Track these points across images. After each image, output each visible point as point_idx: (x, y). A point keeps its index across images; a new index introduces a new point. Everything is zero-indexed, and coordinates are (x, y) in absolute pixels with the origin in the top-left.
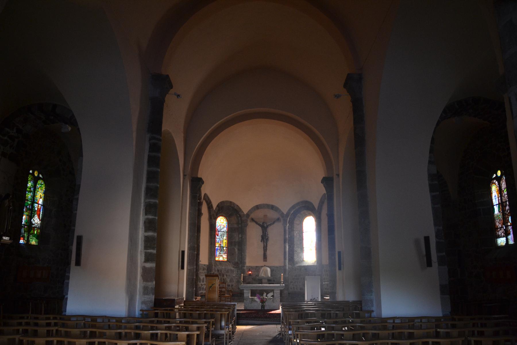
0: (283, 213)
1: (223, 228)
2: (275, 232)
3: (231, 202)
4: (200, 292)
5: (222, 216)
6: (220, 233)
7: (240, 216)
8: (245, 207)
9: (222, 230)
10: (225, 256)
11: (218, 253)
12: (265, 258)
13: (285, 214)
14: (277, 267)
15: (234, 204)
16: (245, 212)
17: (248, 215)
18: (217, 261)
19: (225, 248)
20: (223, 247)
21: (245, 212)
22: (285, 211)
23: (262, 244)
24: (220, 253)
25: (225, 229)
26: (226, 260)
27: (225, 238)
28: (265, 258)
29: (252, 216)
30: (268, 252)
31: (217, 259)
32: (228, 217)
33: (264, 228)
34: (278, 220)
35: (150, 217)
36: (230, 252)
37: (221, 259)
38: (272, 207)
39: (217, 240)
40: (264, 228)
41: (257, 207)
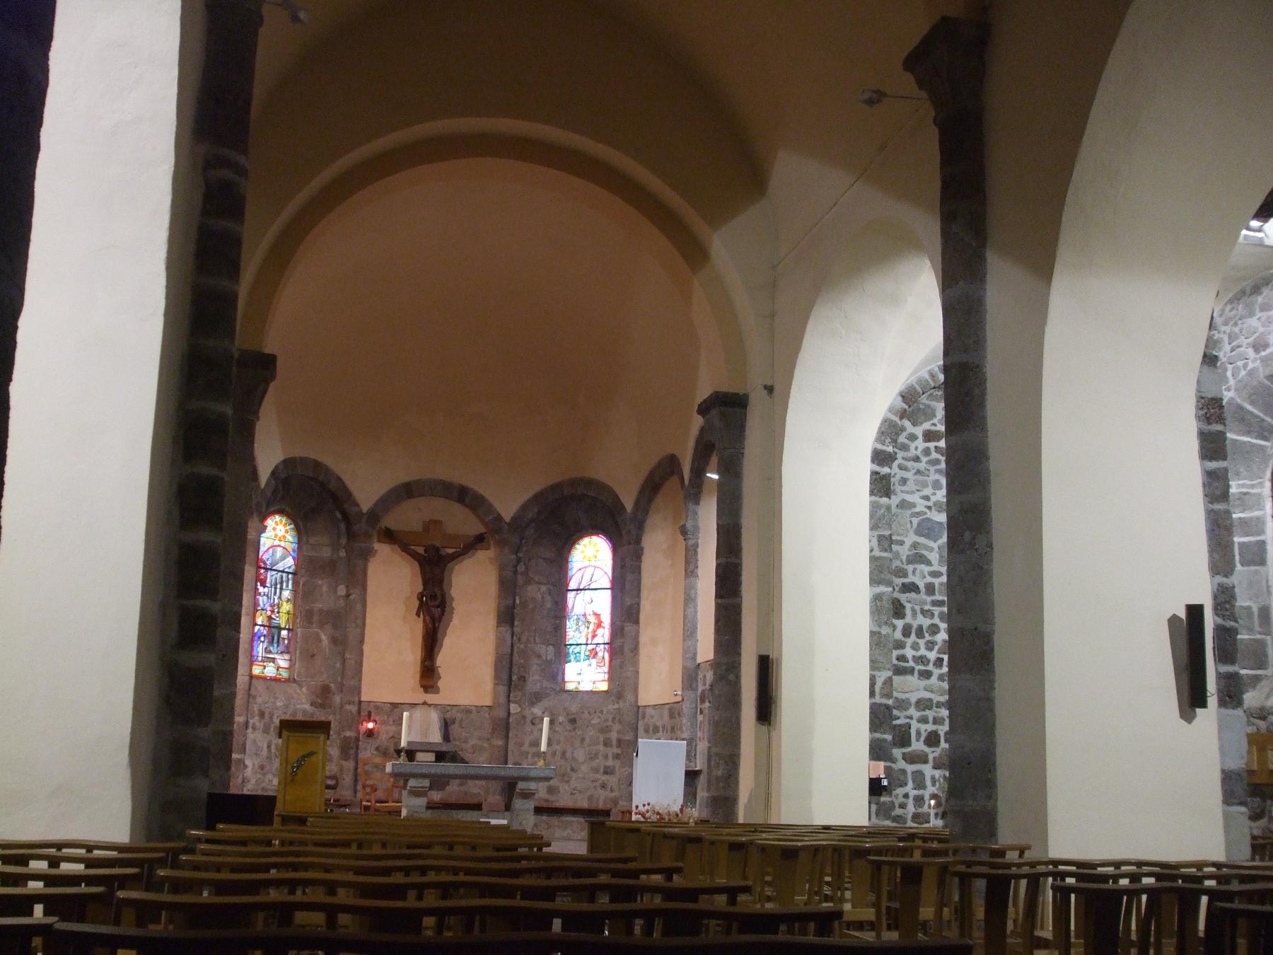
0: (499, 518)
1: (283, 558)
2: (474, 584)
3: (317, 465)
4: (936, 823)
5: (288, 516)
6: (271, 577)
7: (346, 517)
8: (366, 484)
9: (280, 566)
10: (283, 662)
11: (260, 649)
12: (429, 675)
13: (507, 518)
14: (467, 710)
15: (328, 471)
16: (365, 506)
17: (373, 516)
18: (258, 677)
19: (284, 633)
20: (280, 629)
21: (365, 506)
22: (507, 509)
23: (418, 627)
24: (267, 651)
25: (289, 562)
26: (285, 674)
27: (286, 594)
28: (429, 675)
29: (391, 521)
30: (442, 659)
31: (256, 670)
32: (302, 523)
33: (434, 569)
34: (479, 541)
35: (878, 735)
36: (303, 652)
37: (270, 671)
38: (463, 495)
39: (262, 600)
40: (434, 569)
41: (408, 491)
